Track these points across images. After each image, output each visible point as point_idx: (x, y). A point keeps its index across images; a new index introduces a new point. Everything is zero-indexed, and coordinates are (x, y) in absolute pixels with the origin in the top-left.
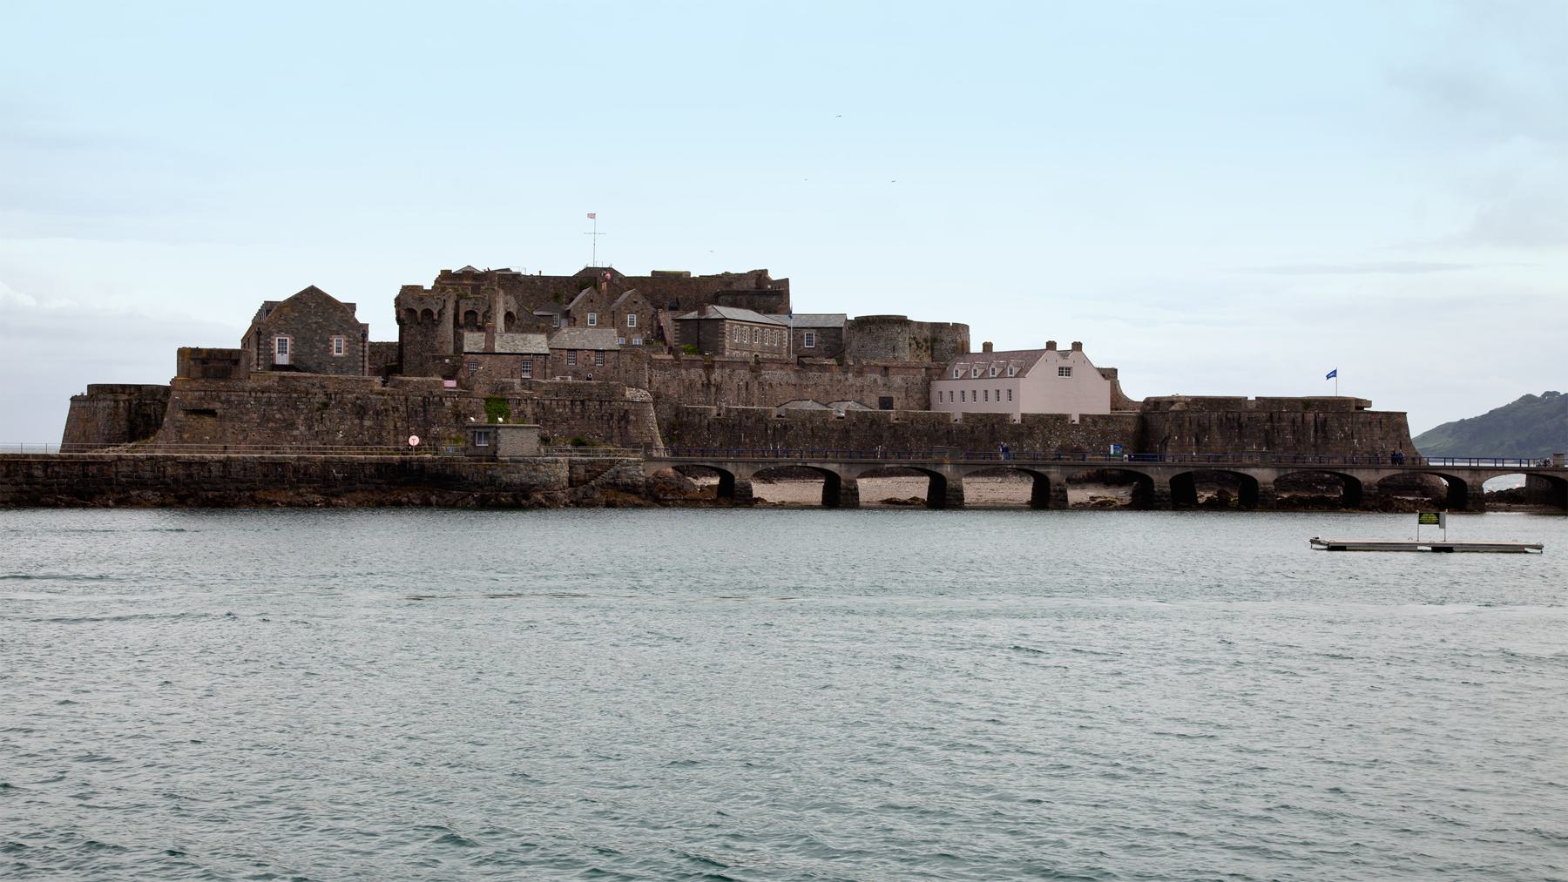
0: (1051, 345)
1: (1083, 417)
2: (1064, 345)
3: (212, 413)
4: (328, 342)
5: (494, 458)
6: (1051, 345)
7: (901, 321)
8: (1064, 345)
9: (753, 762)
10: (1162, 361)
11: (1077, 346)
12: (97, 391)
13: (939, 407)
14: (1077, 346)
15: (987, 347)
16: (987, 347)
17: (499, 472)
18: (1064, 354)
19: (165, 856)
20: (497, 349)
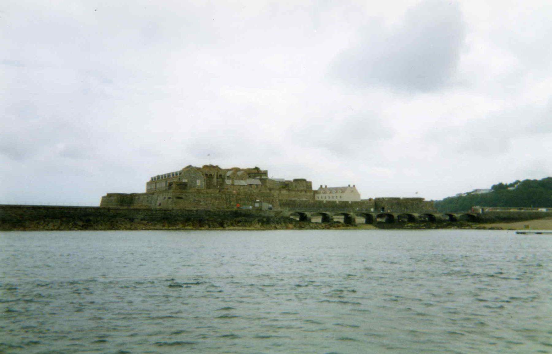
0: (349, 186)
1: (352, 202)
2: (351, 186)
3: (181, 198)
4: (196, 181)
5: (261, 210)
6: (349, 186)
7: (304, 180)
8: (351, 186)
9: (149, 285)
10: (369, 191)
11: (354, 186)
12: (110, 195)
13: (316, 199)
14: (354, 186)
15: (326, 186)
16: (326, 186)
17: (263, 214)
18: (352, 188)
19: (5, 314)
20: (235, 184)
